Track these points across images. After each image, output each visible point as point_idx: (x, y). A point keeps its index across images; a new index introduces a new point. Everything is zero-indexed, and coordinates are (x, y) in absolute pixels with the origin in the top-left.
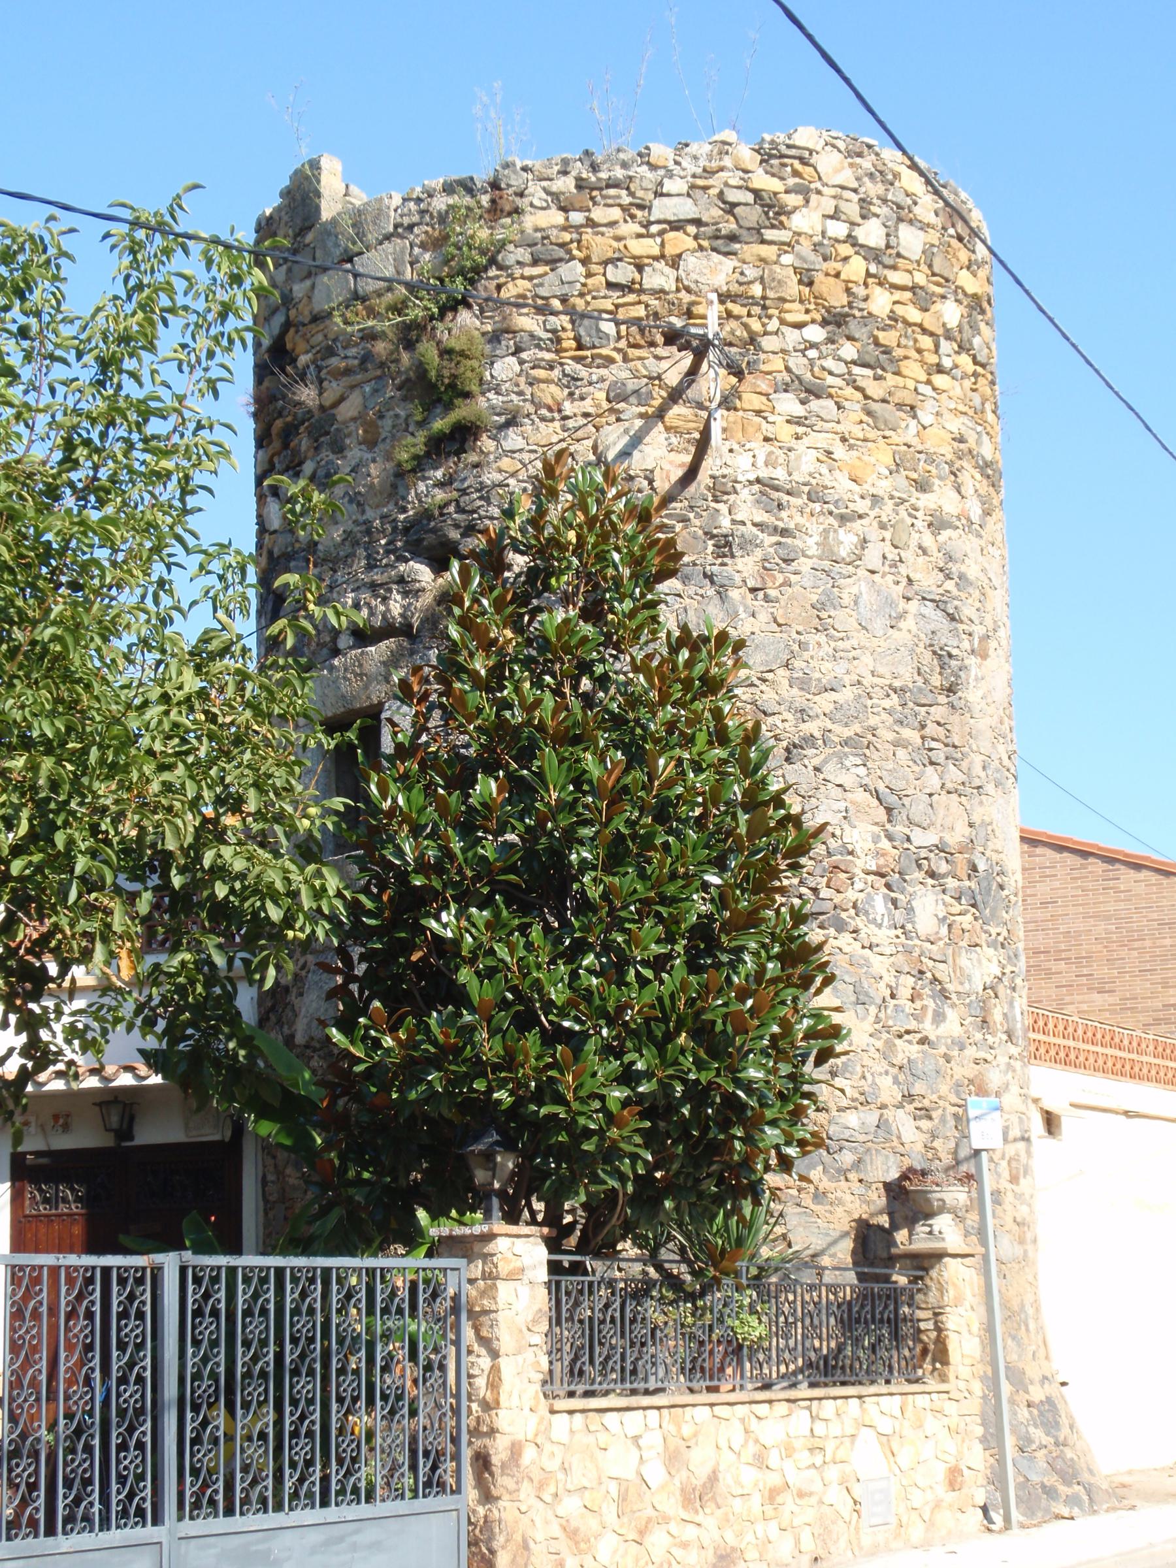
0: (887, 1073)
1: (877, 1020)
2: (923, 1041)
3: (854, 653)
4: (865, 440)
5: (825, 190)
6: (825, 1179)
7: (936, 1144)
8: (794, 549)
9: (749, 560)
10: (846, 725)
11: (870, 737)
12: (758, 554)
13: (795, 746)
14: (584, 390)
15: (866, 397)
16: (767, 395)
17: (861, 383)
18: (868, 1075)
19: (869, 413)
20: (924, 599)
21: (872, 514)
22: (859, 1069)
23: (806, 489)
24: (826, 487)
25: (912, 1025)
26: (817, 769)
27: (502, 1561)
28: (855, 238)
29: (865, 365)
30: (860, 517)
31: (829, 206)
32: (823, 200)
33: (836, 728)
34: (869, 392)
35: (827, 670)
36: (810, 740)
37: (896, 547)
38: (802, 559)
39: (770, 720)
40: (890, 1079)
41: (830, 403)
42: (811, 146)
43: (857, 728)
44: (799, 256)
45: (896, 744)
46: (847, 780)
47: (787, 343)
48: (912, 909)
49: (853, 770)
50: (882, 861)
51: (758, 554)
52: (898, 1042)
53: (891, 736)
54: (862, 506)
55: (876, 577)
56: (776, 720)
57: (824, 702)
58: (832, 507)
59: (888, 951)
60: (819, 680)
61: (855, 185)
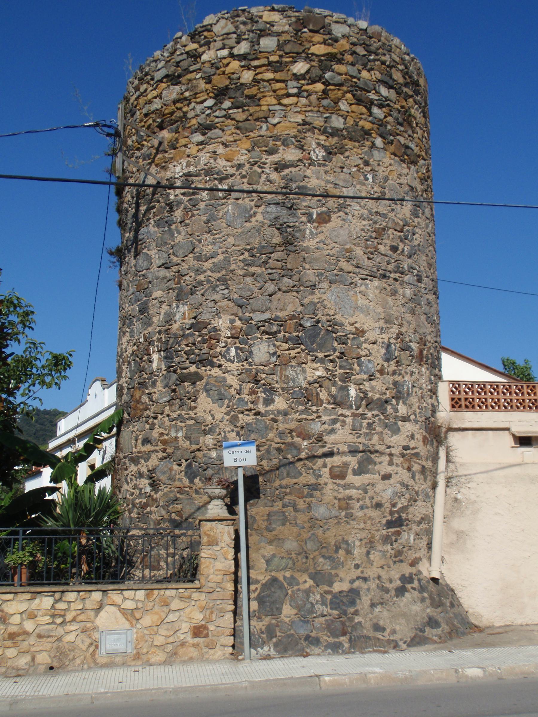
0: (233, 431)
1: (228, 406)
2: (258, 413)
3: (223, 238)
4: (235, 141)
5: (218, 39)
6: (200, 483)
7: (262, 463)
8: (197, 200)
9: (179, 211)
10: (219, 272)
11: (231, 275)
12: (183, 206)
13: (195, 287)
14: (355, 35)
15: (237, 121)
16: (187, 137)
17: (233, 116)
18: (222, 433)
19: (238, 128)
20: (269, 204)
21: (237, 173)
22: (217, 430)
23: (202, 172)
24: (212, 168)
25: (250, 406)
26: (203, 295)
27: (25, 607)
28: (233, 53)
29: (237, 108)
30: (232, 176)
31: (219, 44)
32: (216, 44)
33: (214, 275)
34: (237, 119)
35: (207, 249)
36: (201, 283)
37: (251, 184)
38: (201, 203)
39: (184, 278)
40: (234, 434)
41: (217, 130)
42: (210, 22)
43: (224, 272)
44: (205, 72)
45: (244, 276)
46: (216, 297)
47: (198, 111)
48: (252, 351)
49: (221, 292)
50: (234, 331)
51: (183, 206)
52: (240, 416)
53: (241, 272)
54: (231, 171)
55: (240, 201)
56: (187, 277)
57: (208, 264)
58: (215, 176)
59: (236, 373)
60: (206, 255)
61: (234, 30)
